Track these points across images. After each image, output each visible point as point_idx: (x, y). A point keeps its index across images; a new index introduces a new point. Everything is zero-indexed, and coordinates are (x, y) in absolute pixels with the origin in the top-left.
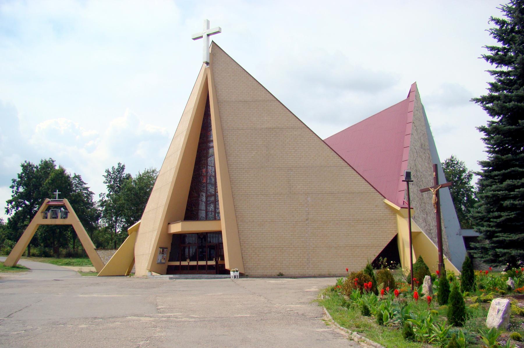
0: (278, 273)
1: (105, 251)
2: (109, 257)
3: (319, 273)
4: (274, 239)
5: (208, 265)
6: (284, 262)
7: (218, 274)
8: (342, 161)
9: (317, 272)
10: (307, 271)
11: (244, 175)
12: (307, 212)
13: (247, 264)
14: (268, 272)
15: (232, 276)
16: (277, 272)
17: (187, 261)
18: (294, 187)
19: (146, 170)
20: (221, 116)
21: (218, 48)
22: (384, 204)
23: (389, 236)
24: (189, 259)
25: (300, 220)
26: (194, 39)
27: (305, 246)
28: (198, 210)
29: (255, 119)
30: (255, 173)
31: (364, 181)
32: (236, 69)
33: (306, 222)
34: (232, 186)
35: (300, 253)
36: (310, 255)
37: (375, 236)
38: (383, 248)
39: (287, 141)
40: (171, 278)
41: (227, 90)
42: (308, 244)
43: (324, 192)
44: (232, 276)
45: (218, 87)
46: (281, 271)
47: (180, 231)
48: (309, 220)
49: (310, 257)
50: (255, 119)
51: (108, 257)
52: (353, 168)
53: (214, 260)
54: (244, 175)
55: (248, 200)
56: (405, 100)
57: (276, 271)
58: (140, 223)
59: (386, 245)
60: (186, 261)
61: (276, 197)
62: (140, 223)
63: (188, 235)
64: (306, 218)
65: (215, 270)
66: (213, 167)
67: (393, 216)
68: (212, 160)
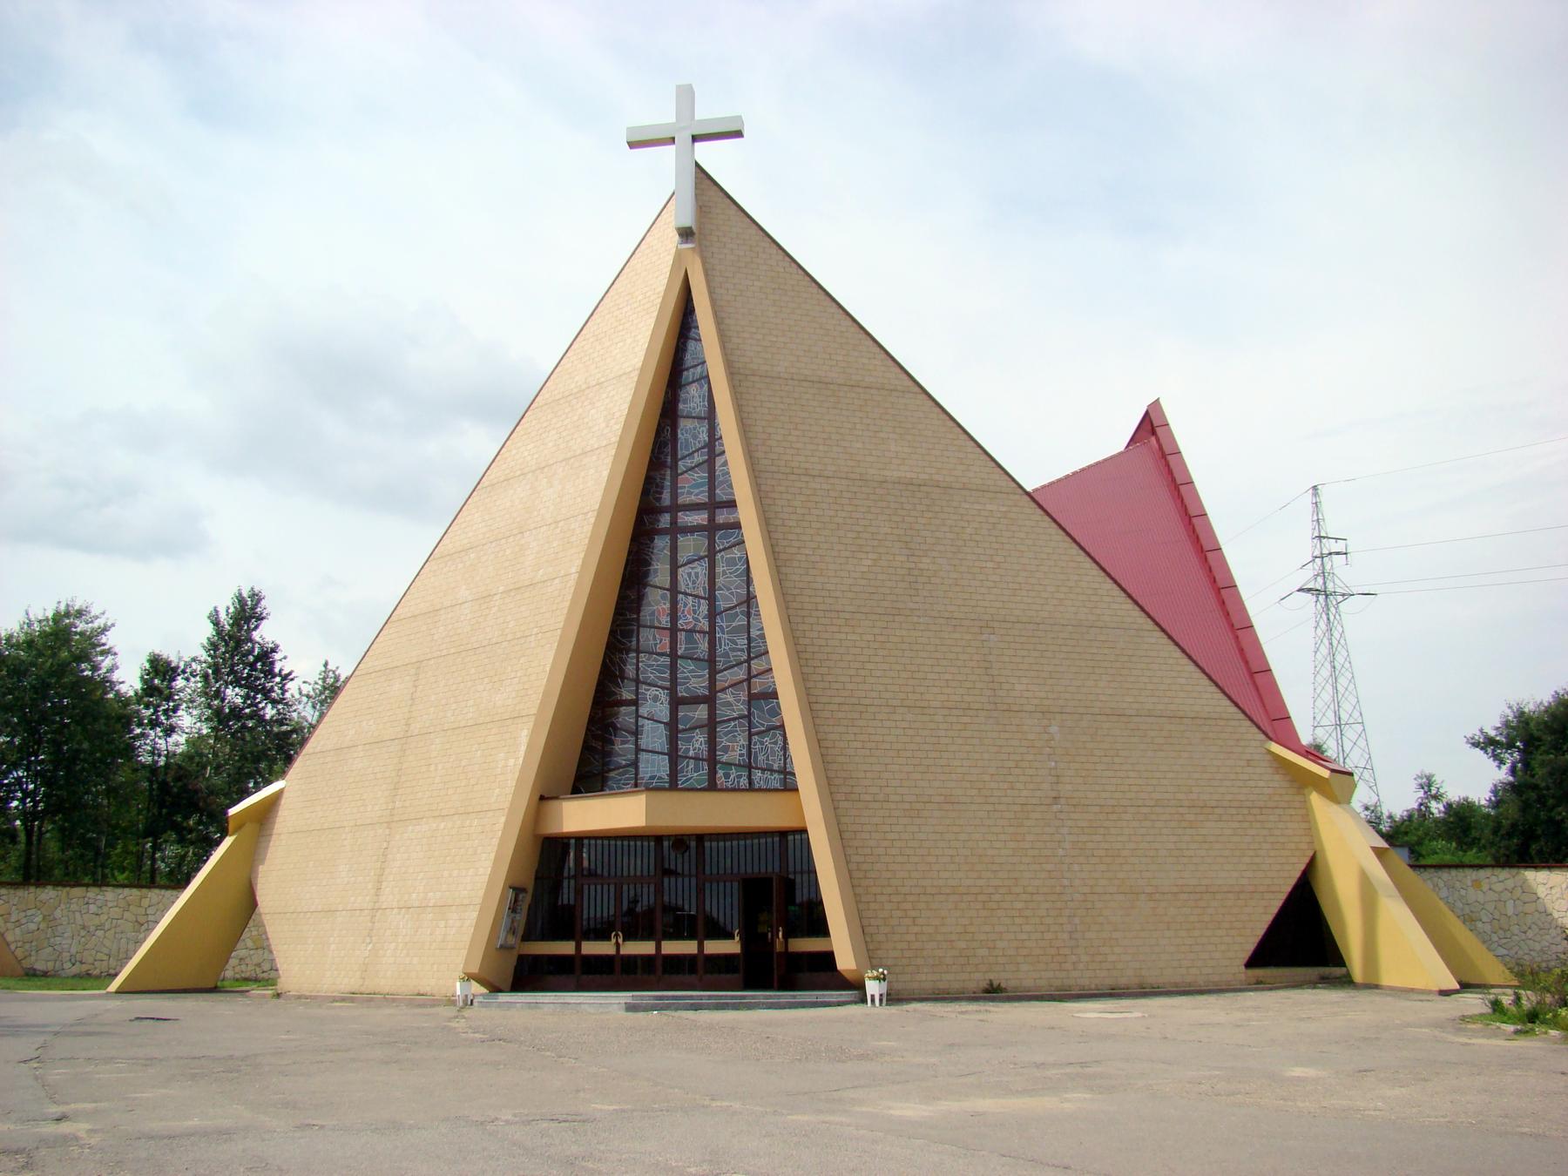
0: (984, 985)
1: (12, 891)
2: (29, 913)
3: (1109, 982)
4: (959, 864)
5: (623, 956)
6: (1000, 944)
7: (779, 989)
8: (1137, 612)
9: (1105, 979)
10: (1075, 974)
11: (843, 636)
12: (1053, 772)
13: (879, 952)
14: (950, 980)
15: (873, 996)
16: (979, 980)
17: (614, 941)
18: (1005, 686)
19: (62, 608)
20: (744, 420)
21: (715, 188)
22: (1268, 757)
23: (1294, 860)
24: (620, 933)
25: (1034, 801)
26: (633, 145)
27: (1058, 890)
28: (623, 748)
29: (859, 445)
30: (877, 631)
31: (1206, 681)
32: (783, 270)
33: (1055, 807)
34: (805, 670)
35: (1045, 914)
36: (1077, 920)
37: (1257, 860)
38: (1282, 897)
39: (968, 531)
40: (631, 1008)
41: (760, 337)
42: (1066, 882)
43: (1096, 711)
44: (873, 996)
45: (727, 321)
46: (992, 976)
47: (643, 827)
48: (1063, 801)
49: (1078, 927)
50: (859, 445)
51: (23, 914)
52: (1170, 637)
53: (737, 938)
54: (843, 636)
55: (861, 723)
56: (1120, 454)
57: (978, 976)
58: (275, 799)
59: (1289, 889)
60: (733, 938)
61: (954, 719)
62: (278, 796)
63: (646, 844)
64: (1054, 794)
65: (736, 975)
66: (702, 598)
67: (1298, 798)
68: (697, 574)
